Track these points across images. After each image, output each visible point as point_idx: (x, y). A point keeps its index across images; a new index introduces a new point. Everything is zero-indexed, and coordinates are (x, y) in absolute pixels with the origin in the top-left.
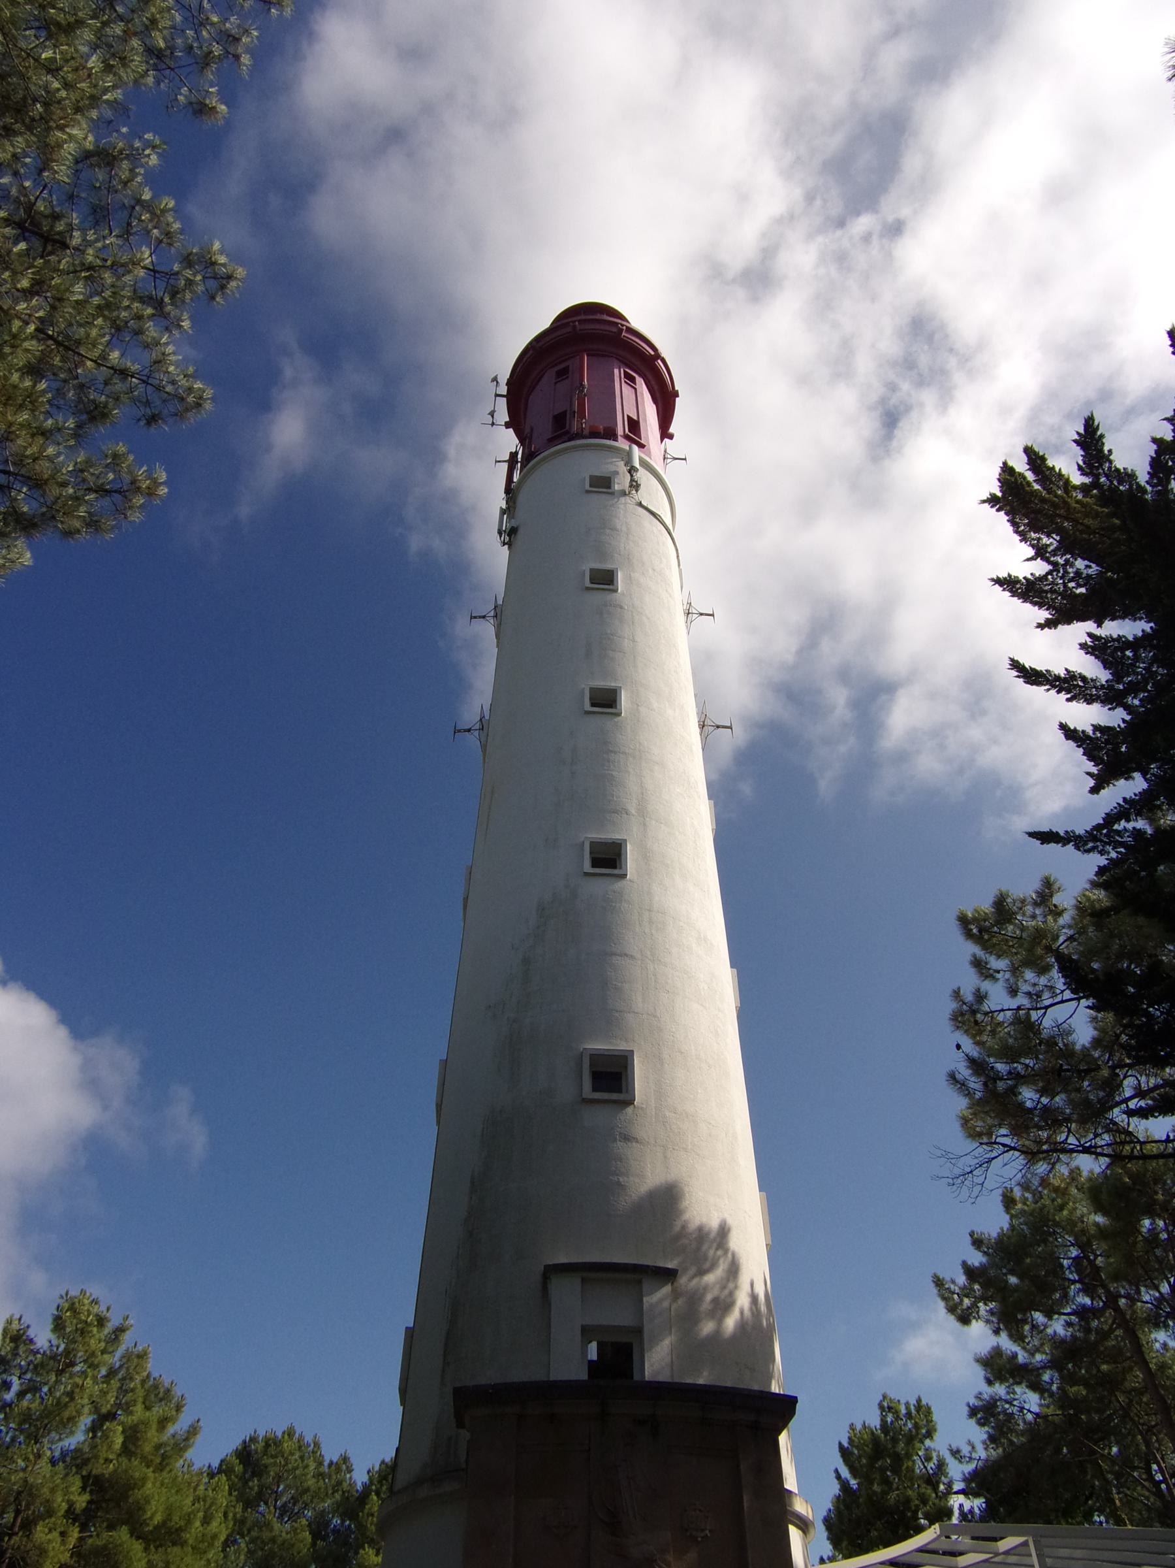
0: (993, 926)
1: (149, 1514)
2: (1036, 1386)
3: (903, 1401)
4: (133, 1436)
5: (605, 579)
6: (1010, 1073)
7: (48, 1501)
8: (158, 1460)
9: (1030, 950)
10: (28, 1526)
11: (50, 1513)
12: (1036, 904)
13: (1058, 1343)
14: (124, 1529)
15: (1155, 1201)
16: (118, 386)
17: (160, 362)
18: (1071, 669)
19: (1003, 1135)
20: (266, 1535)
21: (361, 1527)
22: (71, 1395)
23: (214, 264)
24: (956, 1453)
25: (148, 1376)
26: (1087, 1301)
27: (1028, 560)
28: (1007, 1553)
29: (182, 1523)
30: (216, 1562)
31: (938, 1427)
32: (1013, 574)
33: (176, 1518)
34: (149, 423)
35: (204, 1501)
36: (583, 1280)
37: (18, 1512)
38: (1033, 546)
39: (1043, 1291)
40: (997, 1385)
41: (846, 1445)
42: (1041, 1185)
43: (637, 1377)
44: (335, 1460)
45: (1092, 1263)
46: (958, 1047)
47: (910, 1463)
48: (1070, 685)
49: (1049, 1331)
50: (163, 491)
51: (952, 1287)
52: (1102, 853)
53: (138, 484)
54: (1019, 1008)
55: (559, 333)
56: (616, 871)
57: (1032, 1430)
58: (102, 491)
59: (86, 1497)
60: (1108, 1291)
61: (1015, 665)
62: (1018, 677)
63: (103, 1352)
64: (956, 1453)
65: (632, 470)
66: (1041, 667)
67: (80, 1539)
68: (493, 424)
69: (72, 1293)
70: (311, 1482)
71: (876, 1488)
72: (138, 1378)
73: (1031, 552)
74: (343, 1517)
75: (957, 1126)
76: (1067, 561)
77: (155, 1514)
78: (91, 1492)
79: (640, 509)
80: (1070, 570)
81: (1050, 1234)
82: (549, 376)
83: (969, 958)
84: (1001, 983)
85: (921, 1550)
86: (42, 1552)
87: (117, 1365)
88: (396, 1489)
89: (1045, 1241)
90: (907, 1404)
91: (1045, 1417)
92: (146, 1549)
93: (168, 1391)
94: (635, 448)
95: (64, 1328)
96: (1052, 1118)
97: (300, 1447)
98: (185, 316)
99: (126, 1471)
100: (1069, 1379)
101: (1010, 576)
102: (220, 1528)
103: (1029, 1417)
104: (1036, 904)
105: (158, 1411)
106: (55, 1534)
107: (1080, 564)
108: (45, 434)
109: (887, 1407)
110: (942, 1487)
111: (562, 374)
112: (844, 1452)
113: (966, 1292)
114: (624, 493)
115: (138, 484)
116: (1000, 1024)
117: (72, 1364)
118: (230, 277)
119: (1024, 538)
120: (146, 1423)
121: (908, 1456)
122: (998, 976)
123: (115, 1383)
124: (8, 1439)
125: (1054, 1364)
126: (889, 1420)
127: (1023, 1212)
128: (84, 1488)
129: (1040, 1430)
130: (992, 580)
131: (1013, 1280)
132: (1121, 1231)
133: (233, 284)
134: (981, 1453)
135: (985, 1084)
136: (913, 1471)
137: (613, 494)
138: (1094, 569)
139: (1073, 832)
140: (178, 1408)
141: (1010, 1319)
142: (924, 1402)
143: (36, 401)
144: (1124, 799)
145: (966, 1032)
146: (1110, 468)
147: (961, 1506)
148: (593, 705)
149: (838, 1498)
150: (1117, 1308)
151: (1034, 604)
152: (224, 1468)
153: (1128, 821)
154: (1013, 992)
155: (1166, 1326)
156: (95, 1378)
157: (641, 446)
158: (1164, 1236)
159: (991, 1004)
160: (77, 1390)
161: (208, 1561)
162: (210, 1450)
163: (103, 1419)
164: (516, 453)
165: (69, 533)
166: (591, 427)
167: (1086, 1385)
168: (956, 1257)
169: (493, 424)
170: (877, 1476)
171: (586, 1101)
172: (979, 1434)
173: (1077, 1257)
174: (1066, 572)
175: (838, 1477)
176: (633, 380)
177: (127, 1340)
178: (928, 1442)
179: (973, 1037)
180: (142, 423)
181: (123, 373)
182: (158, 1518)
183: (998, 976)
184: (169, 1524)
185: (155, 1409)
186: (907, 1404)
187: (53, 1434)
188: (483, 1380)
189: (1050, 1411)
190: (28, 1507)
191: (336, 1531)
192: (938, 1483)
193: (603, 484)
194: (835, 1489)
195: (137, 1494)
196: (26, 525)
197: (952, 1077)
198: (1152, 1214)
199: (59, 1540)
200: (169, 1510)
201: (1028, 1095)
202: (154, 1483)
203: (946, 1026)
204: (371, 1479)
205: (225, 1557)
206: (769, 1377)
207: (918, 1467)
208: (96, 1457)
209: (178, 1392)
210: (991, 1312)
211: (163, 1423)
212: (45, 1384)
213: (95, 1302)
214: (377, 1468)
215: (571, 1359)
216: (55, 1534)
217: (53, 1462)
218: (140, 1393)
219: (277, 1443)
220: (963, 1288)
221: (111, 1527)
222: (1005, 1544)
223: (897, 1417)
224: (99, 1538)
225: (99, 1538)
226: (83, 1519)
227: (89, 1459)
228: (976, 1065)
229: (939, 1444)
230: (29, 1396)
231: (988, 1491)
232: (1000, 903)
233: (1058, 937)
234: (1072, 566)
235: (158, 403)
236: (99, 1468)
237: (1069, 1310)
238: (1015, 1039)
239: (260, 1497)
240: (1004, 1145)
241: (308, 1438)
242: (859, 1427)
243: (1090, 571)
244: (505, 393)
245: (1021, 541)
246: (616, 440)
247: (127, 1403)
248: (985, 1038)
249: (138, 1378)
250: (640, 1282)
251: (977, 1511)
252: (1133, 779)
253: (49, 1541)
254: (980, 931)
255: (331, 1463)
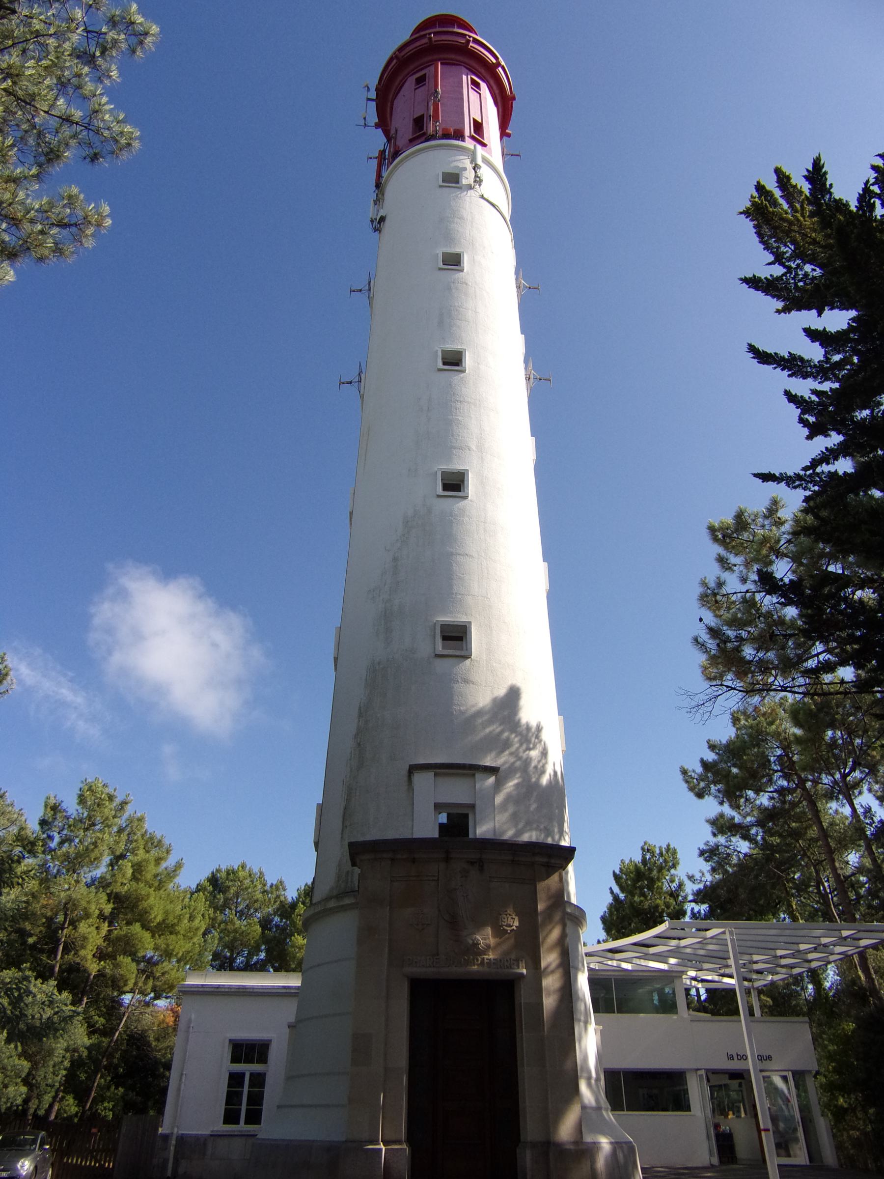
0: (733, 533)
1: (153, 916)
2: (745, 837)
3: (657, 846)
4: (138, 869)
5: (454, 261)
6: (736, 637)
7: (85, 908)
8: (156, 884)
9: (758, 551)
10: (74, 923)
11: (87, 916)
12: (766, 517)
13: (762, 810)
14: (138, 925)
15: (836, 720)
16: (66, 131)
17: (97, 112)
18: (792, 352)
19: (729, 679)
20: (230, 927)
21: (294, 924)
22: (95, 844)
23: (133, 23)
24: (691, 878)
25: (146, 832)
26: (785, 783)
27: (769, 264)
28: (712, 938)
29: (176, 921)
30: (200, 944)
31: (680, 862)
32: (757, 275)
33: (171, 918)
34: (92, 161)
35: (189, 908)
36: (435, 774)
37: (66, 915)
38: (772, 253)
39: (755, 778)
40: (720, 837)
41: (618, 872)
42: (754, 711)
43: (471, 836)
44: (274, 883)
45: (790, 759)
46: (701, 620)
47: (660, 884)
48: (794, 365)
49: (758, 802)
50: (108, 222)
51: (693, 774)
52: (805, 489)
53: (89, 219)
54: (747, 591)
55: (418, 44)
56: (460, 494)
57: (741, 866)
58: (61, 225)
59: (111, 906)
60: (799, 777)
61: (752, 349)
62: (753, 358)
63: (114, 817)
64: (691, 878)
65: (476, 167)
66: (770, 350)
67: (110, 931)
68: (365, 125)
69: (89, 780)
70: (259, 896)
71: (636, 899)
72: (139, 834)
73: (771, 258)
74: (282, 916)
75: (699, 671)
76: (798, 265)
77: (157, 915)
78: (114, 903)
79: (482, 201)
80: (800, 273)
81: (763, 741)
82: (411, 81)
83: (715, 556)
84: (736, 574)
85: (656, 937)
86: (85, 938)
87: (124, 825)
88: (314, 901)
89: (758, 745)
90: (660, 848)
91: (751, 856)
92: (153, 936)
93: (160, 841)
94: (479, 147)
95: (86, 802)
96: (764, 667)
97: (250, 875)
98: (114, 67)
99: (136, 891)
100: (769, 832)
101: (754, 276)
102: (201, 924)
103: (741, 856)
104: (766, 517)
105: (154, 853)
106: (93, 928)
107: (808, 268)
108: (15, 180)
109: (647, 849)
110: (680, 898)
111: (421, 81)
112: (615, 876)
113: (701, 778)
114: (470, 187)
115: (89, 219)
116: (734, 602)
117: (94, 825)
118: (146, 34)
119: (767, 247)
120: (147, 861)
121: (659, 879)
122: (735, 568)
123: (124, 837)
124: (55, 871)
125: (760, 823)
126: (648, 857)
127: (745, 727)
128: (109, 901)
129: (747, 865)
130: (741, 279)
131: (735, 770)
132: (812, 739)
133: (149, 39)
134: (708, 878)
135: (718, 645)
136: (662, 888)
137: (460, 188)
138: (818, 272)
139: (785, 474)
140: (168, 852)
141: (731, 795)
142: (672, 846)
143: (6, 154)
144: (826, 448)
145: (709, 608)
146: (830, 198)
147: (693, 909)
148: (444, 364)
149: (611, 905)
150: (804, 789)
151: (773, 297)
152: (200, 888)
153: (828, 464)
154: (744, 580)
155: (837, 799)
156: (110, 833)
157: (484, 145)
158: (840, 742)
159: (727, 589)
160: (99, 841)
161: (194, 944)
162: (191, 877)
163: (117, 858)
164: (384, 151)
165: (41, 259)
166: (443, 129)
167: (780, 836)
168: (696, 755)
169: (365, 125)
170: (638, 891)
171: (438, 656)
172: (706, 867)
173: (781, 755)
174: (797, 274)
175: (612, 892)
176: (477, 85)
177: (129, 810)
178: (673, 871)
179: (714, 611)
180: (88, 160)
181: (67, 120)
182: (159, 919)
183: (735, 568)
184: (167, 922)
185: (152, 852)
186: (660, 848)
187: (85, 868)
188: (368, 838)
189: (755, 852)
190: (72, 912)
191: (277, 926)
192: (678, 896)
193: (452, 179)
194: (609, 899)
195: (144, 905)
196: (12, 256)
197: (696, 640)
198: (832, 725)
199: (96, 932)
200: (166, 913)
201: (748, 652)
202: (155, 898)
203: (695, 603)
204: (299, 895)
205: (205, 941)
206: (561, 832)
207: (665, 887)
208: (116, 882)
209: (166, 842)
210: (719, 791)
211: (158, 861)
212: (77, 837)
213: (105, 786)
214: (303, 888)
215: (427, 825)
216: (93, 928)
217: (88, 886)
218: (141, 843)
219: (234, 872)
220: (700, 775)
221: (129, 923)
222: (710, 934)
223: (653, 856)
224: (121, 929)
225: (121, 929)
226: (111, 919)
227: (110, 883)
228: (713, 632)
229: (680, 873)
230: (66, 845)
231: (710, 900)
232: (739, 516)
233: (779, 541)
234: (801, 270)
235: (98, 144)
236: (118, 889)
237: (772, 789)
238: (744, 614)
239: (226, 905)
240: (727, 687)
241: (256, 870)
242: (627, 862)
243: (815, 274)
244: (374, 97)
245: (764, 249)
246: (463, 141)
247: (133, 849)
248: (722, 612)
249: (139, 834)
250: (474, 775)
251: (703, 912)
252: (830, 436)
253: (89, 933)
254: (724, 537)
255: (272, 886)
